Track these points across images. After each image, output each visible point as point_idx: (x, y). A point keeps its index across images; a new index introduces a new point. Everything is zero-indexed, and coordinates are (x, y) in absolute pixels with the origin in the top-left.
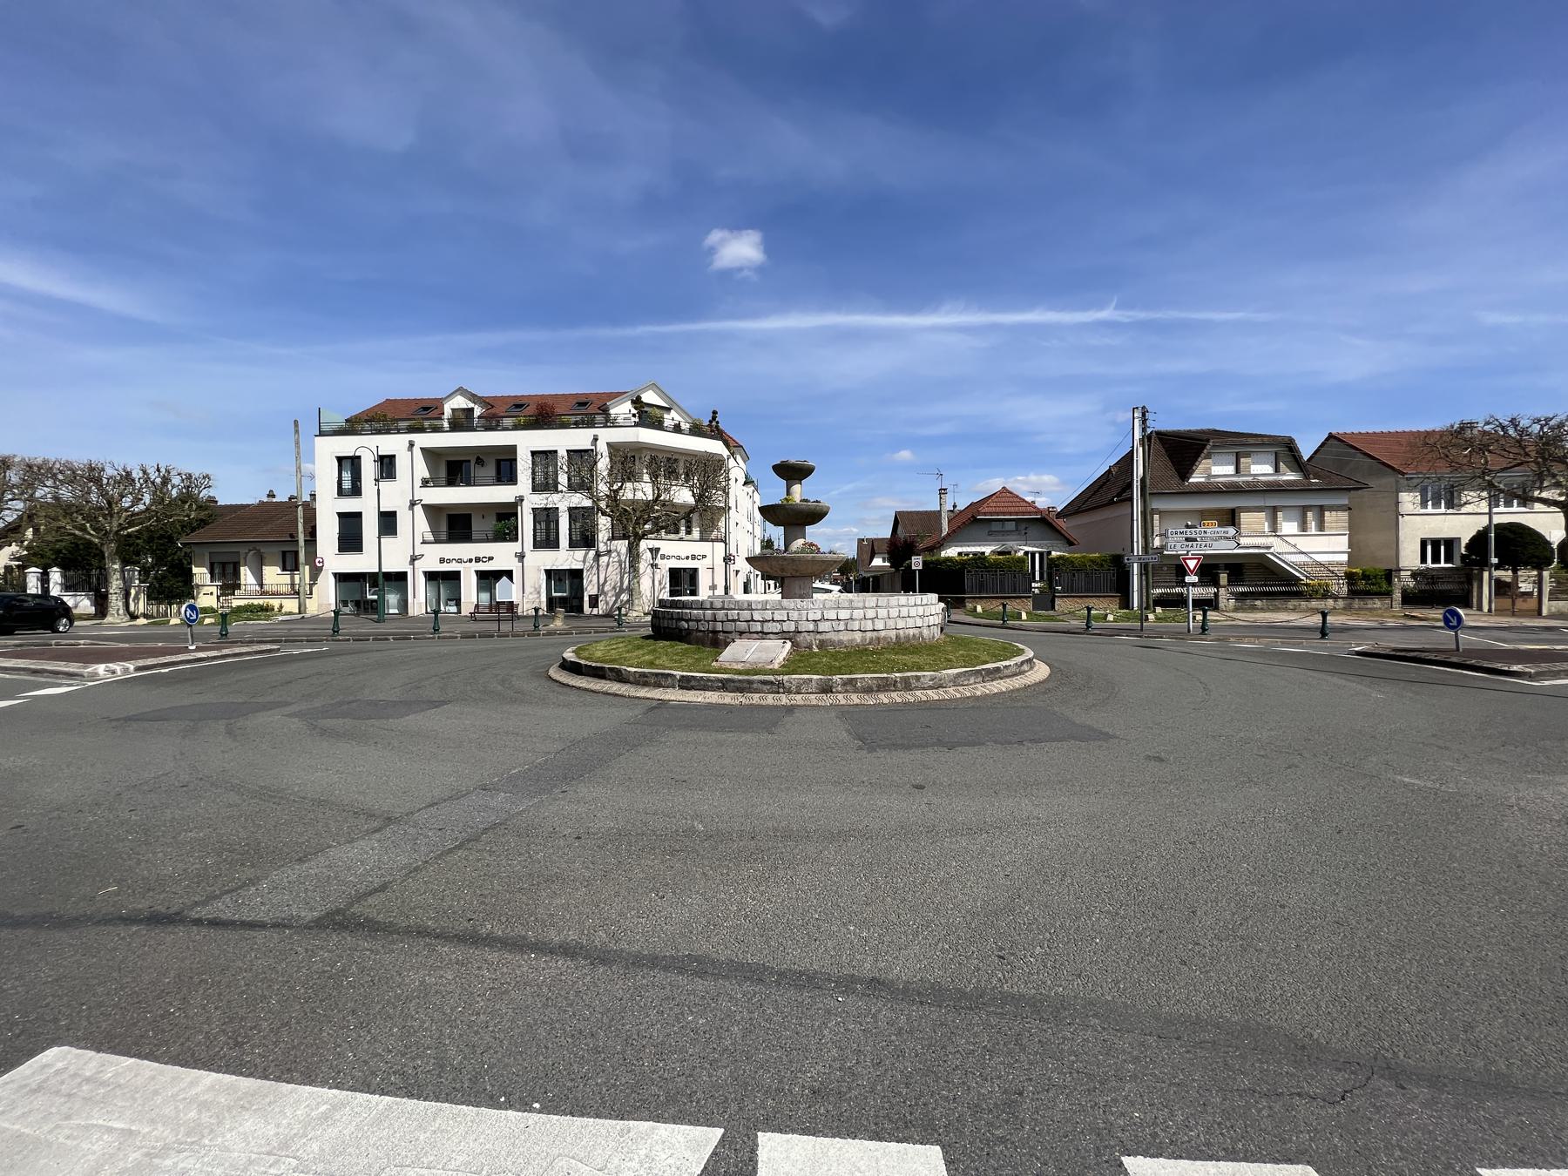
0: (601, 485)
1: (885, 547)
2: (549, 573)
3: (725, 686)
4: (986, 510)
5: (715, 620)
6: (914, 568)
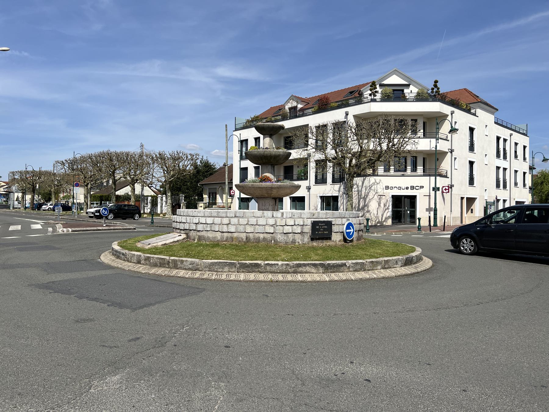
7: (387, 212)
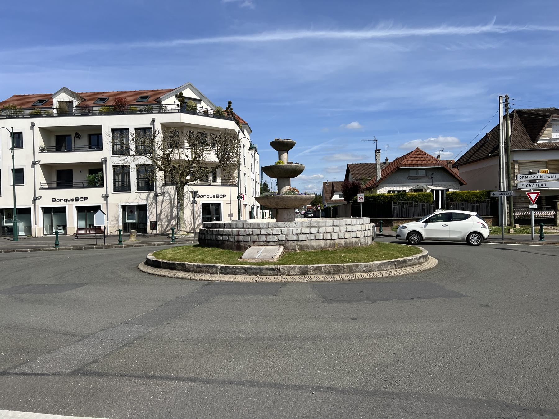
0: (158, 151)
1: (340, 188)
2: (124, 207)
3: (246, 272)
4: (406, 163)
5: (239, 235)
6: (359, 201)
7: (199, 219)
